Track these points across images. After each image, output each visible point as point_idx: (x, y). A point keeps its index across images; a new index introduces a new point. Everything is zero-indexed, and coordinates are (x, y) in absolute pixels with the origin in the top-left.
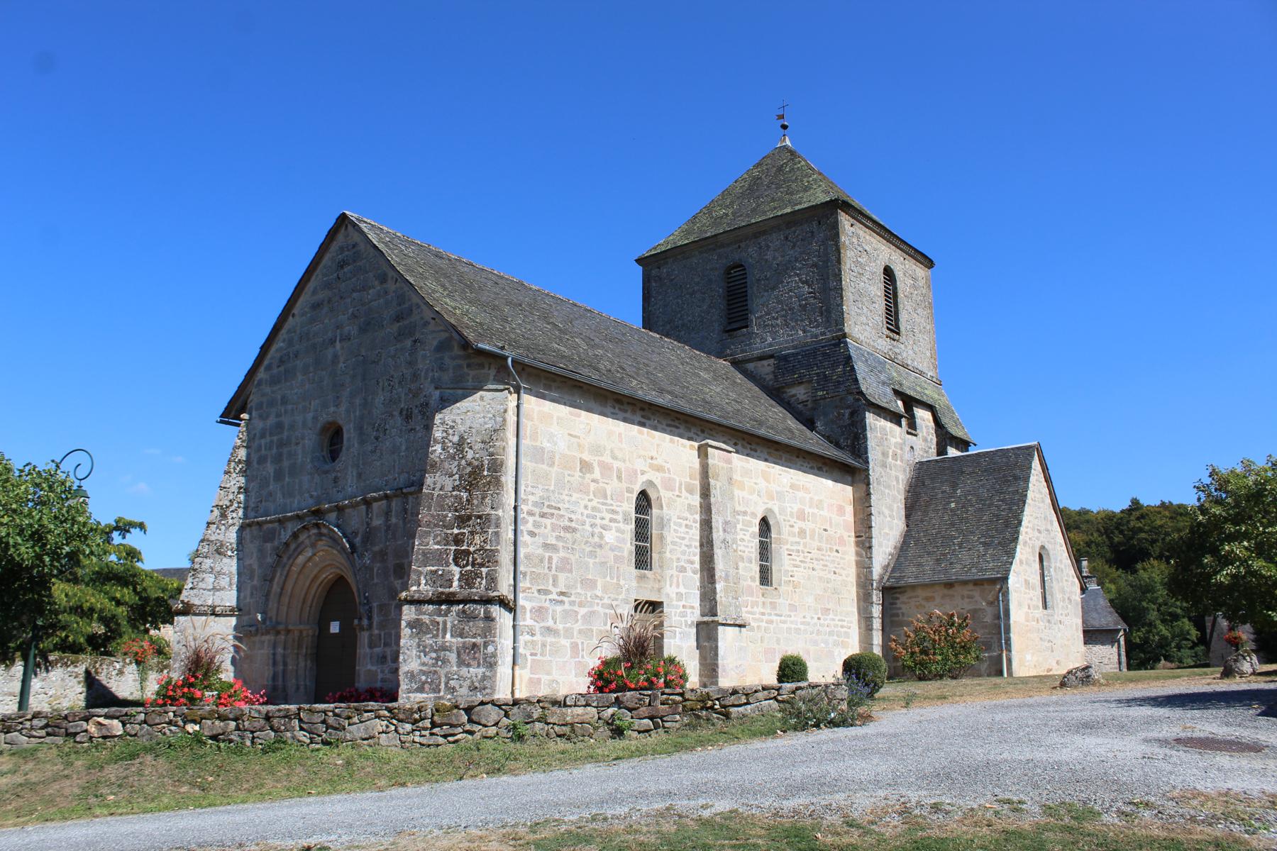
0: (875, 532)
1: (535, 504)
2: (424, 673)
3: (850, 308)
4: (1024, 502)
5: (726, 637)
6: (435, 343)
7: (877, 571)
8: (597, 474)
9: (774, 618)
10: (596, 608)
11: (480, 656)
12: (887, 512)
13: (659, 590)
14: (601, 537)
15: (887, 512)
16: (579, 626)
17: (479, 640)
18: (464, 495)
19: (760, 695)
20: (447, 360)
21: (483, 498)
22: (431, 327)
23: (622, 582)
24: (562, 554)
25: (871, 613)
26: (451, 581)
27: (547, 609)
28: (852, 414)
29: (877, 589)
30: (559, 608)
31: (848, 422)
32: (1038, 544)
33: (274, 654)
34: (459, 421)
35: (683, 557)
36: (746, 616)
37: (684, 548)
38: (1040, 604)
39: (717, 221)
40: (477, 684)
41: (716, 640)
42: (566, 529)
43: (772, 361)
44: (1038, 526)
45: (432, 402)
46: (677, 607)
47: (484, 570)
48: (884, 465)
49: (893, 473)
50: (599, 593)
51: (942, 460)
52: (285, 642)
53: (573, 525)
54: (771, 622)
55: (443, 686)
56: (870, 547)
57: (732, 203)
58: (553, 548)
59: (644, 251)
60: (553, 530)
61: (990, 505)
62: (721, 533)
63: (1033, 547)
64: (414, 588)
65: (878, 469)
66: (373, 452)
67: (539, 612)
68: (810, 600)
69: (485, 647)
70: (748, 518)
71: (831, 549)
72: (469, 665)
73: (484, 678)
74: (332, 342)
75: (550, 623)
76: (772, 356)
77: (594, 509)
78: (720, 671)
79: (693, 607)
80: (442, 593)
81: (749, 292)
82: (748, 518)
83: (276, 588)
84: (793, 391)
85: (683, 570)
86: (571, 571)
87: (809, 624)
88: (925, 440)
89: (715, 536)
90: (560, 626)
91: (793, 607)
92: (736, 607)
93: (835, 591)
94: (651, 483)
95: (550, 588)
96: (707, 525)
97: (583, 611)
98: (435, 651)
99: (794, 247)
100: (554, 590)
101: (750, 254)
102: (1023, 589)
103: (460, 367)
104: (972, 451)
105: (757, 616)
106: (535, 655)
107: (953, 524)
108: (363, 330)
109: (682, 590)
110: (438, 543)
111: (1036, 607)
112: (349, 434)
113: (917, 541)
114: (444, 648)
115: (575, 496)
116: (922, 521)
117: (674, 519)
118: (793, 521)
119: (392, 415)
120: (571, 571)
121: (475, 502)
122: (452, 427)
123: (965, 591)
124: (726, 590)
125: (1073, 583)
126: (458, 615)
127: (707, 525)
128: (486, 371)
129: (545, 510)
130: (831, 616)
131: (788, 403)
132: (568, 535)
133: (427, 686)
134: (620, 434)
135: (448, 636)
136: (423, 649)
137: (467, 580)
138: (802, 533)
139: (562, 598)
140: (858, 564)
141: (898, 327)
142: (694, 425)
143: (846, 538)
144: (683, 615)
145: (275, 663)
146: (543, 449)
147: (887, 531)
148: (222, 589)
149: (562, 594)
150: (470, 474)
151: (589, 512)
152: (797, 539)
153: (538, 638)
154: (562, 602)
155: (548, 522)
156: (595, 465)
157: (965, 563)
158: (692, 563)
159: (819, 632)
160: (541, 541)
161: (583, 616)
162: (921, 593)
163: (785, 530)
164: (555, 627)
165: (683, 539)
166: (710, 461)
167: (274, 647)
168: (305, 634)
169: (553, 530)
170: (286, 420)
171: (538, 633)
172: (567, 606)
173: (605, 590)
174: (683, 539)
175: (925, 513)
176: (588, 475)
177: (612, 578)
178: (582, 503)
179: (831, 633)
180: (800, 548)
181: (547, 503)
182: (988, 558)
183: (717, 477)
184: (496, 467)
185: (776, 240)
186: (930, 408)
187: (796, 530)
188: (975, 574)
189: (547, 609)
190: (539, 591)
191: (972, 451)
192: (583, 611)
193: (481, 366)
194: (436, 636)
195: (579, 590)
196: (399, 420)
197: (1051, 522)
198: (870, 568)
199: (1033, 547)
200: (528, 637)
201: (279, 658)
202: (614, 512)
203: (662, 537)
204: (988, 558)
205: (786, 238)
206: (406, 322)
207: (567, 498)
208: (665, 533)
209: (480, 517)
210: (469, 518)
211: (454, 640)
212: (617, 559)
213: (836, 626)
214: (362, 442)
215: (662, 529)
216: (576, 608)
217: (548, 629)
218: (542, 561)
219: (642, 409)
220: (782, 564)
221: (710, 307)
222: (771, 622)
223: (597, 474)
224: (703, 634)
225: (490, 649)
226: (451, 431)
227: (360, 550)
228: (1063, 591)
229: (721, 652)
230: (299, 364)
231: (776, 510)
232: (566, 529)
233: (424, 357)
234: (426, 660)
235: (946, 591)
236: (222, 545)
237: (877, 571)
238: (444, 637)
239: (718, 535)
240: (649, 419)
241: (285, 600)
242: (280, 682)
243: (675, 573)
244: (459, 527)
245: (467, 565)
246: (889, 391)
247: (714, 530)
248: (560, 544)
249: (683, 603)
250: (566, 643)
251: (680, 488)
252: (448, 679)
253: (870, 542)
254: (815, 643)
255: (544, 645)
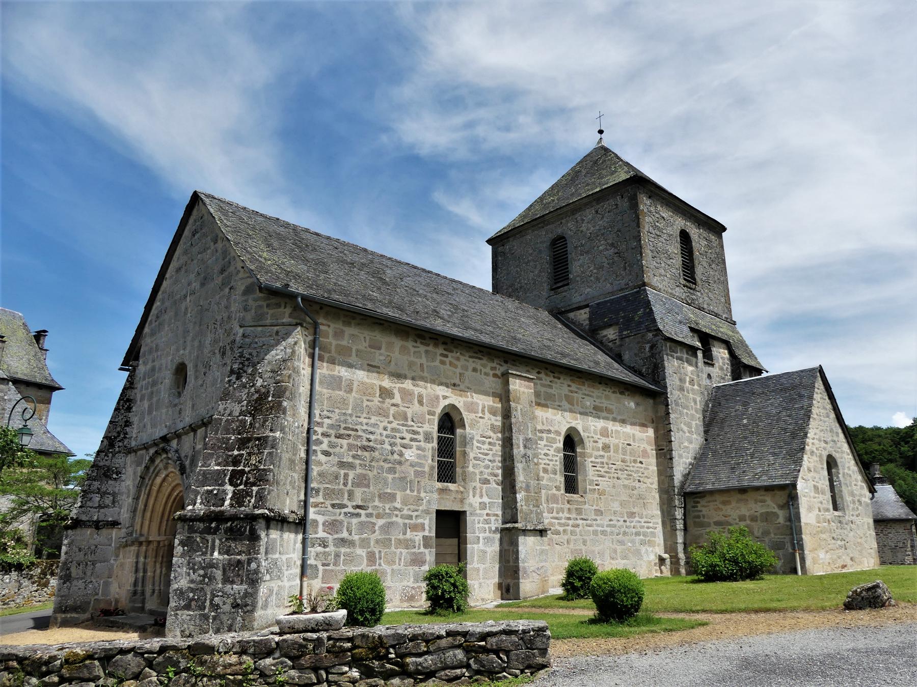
0: (675, 445)
1: (331, 426)
2: (192, 590)
3: (648, 261)
4: (809, 418)
5: (527, 545)
6: (243, 288)
7: (678, 478)
8: (397, 399)
9: (580, 522)
10: (394, 519)
11: (243, 573)
12: (685, 429)
13: (462, 501)
14: (401, 454)
15: (685, 429)
16: (377, 535)
17: (243, 557)
18: (249, 419)
19: (444, 643)
20: (251, 302)
21: (265, 421)
22: (241, 275)
23: (423, 495)
24: (359, 471)
25: (674, 515)
26: (223, 500)
27: (341, 522)
28: (652, 348)
29: (679, 494)
30: (355, 521)
31: (648, 354)
32: (825, 454)
33: (137, 563)
34: (255, 354)
35: (486, 471)
36: (547, 520)
37: (487, 462)
38: (831, 507)
39: (546, 206)
40: (239, 601)
41: (517, 545)
42: (364, 448)
43: (587, 310)
44: (822, 437)
45: (238, 339)
46: (481, 515)
47: (255, 489)
48: (682, 389)
49: (691, 395)
50: (398, 505)
51: (736, 384)
52: (146, 551)
53: (371, 444)
54: (578, 526)
55: (208, 603)
56: (671, 459)
57: (558, 192)
58: (351, 466)
59: (492, 234)
60: (349, 450)
61: (778, 420)
62: (522, 448)
63: (821, 456)
64: (190, 507)
65: (677, 393)
66: (202, 385)
67: (333, 526)
68: (616, 506)
69: (249, 564)
70: (552, 435)
71: (635, 461)
72: (233, 582)
73: (246, 594)
74: (185, 297)
75: (345, 534)
76: (587, 306)
77: (393, 430)
78: (521, 574)
79: (497, 515)
80: (213, 512)
81: (570, 257)
82: (552, 435)
83: (141, 506)
84: (605, 332)
85: (486, 482)
86: (368, 486)
87: (615, 526)
88: (721, 369)
89: (515, 451)
90: (356, 538)
91: (599, 512)
92: (537, 514)
93: (640, 497)
94: (453, 407)
95: (346, 502)
96: (507, 443)
97: (380, 522)
98: (203, 568)
99: (603, 218)
100: (349, 504)
101: (568, 227)
102: (812, 494)
103: (261, 307)
104: (764, 375)
105: (563, 521)
106: (328, 565)
107: (745, 438)
108: (203, 285)
109: (486, 499)
110: (218, 464)
111: (828, 510)
112: (190, 372)
113: (715, 452)
114: (212, 565)
115: (373, 420)
116: (718, 435)
117: (477, 437)
118: (596, 437)
119: (214, 353)
120: (368, 486)
121: (257, 425)
122: (248, 359)
123: (759, 495)
124: (527, 499)
125: (862, 488)
126: (226, 532)
127: (507, 443)
128: (282, 309)
129: (342, 432)
130: (637, 519)
131: (601, 343)
132: (366, 454)
133: (193, 603)
134: (421, 365)
135: (216, 554)
136: (192, 567)
137: (238, 498)
138: (606, 447)
139: (358, 511)
140: (660, 473)
141: (695, 279)
142: (354, 318)
143: (649, 451)
144: (487, 522)
145: (137, 571)
146: (340, 378)
147: (686, 444)
148: (107, 506)
149: (358, 507)
150: (256, 401)
151: (388, 432)
152: (602, 453)
153: (331, 549)
154: (358, 515)
155: (344, 442)
156: (396, 392)
157: (764, 470)
158: (496, 476)
159: (625, 533)
160: (337, 459)
161: (381, 527)
162: (719, 498)
163: (589, 444)
164: (350, 538)
165: (487, 454)
166: (511, 387)
167: (137, 557)
168: (161, 544)
169: (349, 450)
170: (157, 364)
171: (331, 543)
172: (363, 518)
173: (405, 502)
174: (487, 454)
175: (722, 428)
176: (388, 400)
177: (412, 491)
178: (382, 425)
179: (638, 534)
180: (605, 460)
181: (343, 426)
182: (777, 466)
183: (517, 401)
184: (280, 393)
185: (589, 214)
186: (727, 344)
187: (600, 445)
188: (765, 481)
189: (341, 522)
190: (333, 506)
191: (764, 375)
192: (380, 522)
193: (278, 305)
194: (204, 554)
195: (377, 503)
196: (218, 356)
197: (837, 434)
198: (671, 477)
199: (821, 456)
200: (320, 549)
201: (141, 566)
202: (415, 433)
203: (464, 453)
204: (777, 466)
205: (597, 212)
206: (226, 273)
207: (365, 421)
208: (468, 450)
209: (259, 439)
210: (249, 440)
211: (221, 557)
212: (417, 474)
213: (642, 527)
214: (196, 378)
215: (465, 446)
216: (373, 520)
217: (343, 540)
218: (337, 477)
219: (444, 343)
220: (589, 472)
221: (540, 271)
222: (578, 526)
223: (397, 399)
224: (506, 539)
225: (253, 565)
226: (246, 363)
227: (188, 470)
228: (852, 494)
229: (522, 556)
230: (166, 317)
231: (580, 428)
232: (364, 448)
233: (235, 301)
234: (193, 577)
235: (739, 496)
236: (108, 470)
237: (678, 478)
238: (212, 555)
239: (518, 451)
240: (451, 351)
241: (148, 514)
242: (139, 588)
243: (478, 485)
244: (239, 449)
245: (240, 484)
246: (686, 329)
247: (515, 447)
248: (357, 462)
249: (487, 511)
250: (361, 552)
251: (483, 411)
252: (213, 596)
253: (671, 454)
254: (622, 543)
255: (337, 555)
